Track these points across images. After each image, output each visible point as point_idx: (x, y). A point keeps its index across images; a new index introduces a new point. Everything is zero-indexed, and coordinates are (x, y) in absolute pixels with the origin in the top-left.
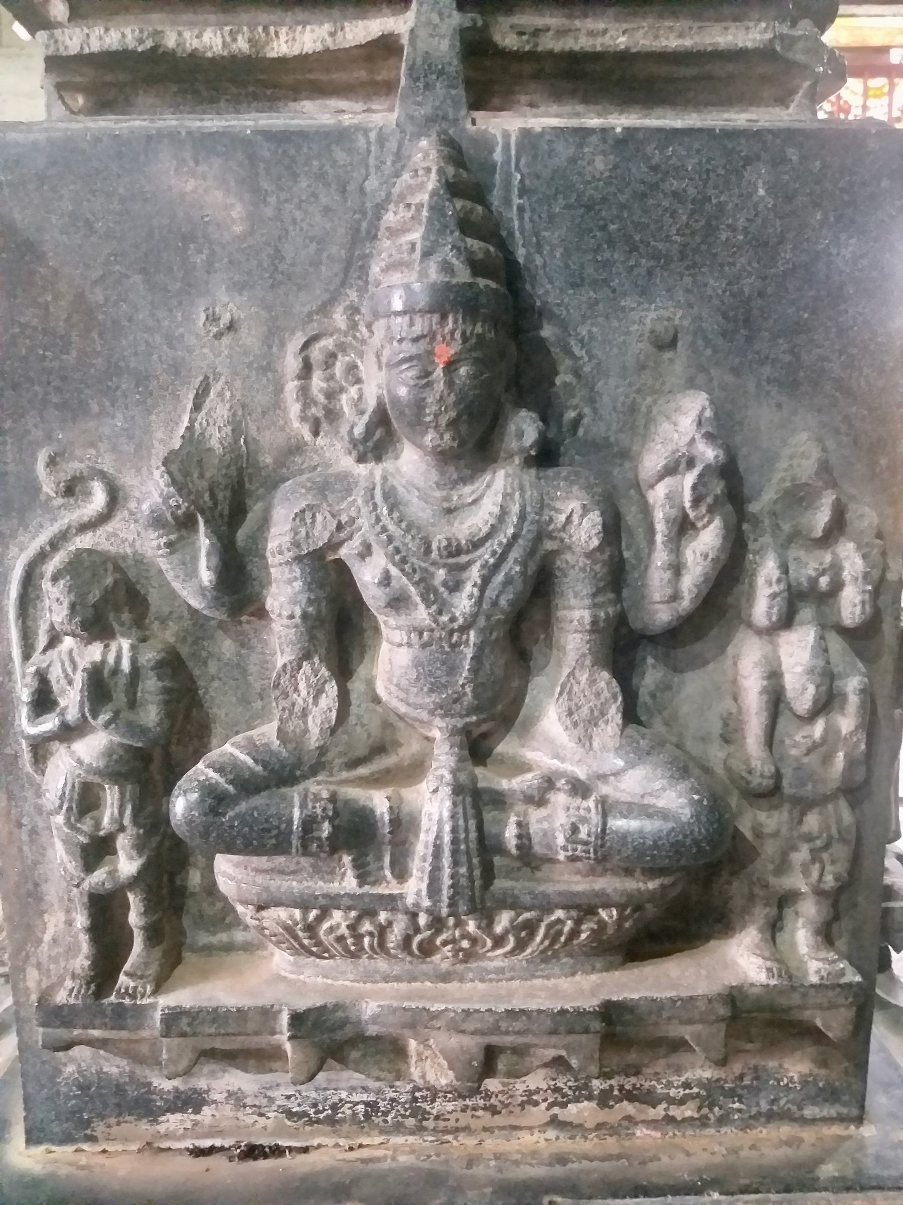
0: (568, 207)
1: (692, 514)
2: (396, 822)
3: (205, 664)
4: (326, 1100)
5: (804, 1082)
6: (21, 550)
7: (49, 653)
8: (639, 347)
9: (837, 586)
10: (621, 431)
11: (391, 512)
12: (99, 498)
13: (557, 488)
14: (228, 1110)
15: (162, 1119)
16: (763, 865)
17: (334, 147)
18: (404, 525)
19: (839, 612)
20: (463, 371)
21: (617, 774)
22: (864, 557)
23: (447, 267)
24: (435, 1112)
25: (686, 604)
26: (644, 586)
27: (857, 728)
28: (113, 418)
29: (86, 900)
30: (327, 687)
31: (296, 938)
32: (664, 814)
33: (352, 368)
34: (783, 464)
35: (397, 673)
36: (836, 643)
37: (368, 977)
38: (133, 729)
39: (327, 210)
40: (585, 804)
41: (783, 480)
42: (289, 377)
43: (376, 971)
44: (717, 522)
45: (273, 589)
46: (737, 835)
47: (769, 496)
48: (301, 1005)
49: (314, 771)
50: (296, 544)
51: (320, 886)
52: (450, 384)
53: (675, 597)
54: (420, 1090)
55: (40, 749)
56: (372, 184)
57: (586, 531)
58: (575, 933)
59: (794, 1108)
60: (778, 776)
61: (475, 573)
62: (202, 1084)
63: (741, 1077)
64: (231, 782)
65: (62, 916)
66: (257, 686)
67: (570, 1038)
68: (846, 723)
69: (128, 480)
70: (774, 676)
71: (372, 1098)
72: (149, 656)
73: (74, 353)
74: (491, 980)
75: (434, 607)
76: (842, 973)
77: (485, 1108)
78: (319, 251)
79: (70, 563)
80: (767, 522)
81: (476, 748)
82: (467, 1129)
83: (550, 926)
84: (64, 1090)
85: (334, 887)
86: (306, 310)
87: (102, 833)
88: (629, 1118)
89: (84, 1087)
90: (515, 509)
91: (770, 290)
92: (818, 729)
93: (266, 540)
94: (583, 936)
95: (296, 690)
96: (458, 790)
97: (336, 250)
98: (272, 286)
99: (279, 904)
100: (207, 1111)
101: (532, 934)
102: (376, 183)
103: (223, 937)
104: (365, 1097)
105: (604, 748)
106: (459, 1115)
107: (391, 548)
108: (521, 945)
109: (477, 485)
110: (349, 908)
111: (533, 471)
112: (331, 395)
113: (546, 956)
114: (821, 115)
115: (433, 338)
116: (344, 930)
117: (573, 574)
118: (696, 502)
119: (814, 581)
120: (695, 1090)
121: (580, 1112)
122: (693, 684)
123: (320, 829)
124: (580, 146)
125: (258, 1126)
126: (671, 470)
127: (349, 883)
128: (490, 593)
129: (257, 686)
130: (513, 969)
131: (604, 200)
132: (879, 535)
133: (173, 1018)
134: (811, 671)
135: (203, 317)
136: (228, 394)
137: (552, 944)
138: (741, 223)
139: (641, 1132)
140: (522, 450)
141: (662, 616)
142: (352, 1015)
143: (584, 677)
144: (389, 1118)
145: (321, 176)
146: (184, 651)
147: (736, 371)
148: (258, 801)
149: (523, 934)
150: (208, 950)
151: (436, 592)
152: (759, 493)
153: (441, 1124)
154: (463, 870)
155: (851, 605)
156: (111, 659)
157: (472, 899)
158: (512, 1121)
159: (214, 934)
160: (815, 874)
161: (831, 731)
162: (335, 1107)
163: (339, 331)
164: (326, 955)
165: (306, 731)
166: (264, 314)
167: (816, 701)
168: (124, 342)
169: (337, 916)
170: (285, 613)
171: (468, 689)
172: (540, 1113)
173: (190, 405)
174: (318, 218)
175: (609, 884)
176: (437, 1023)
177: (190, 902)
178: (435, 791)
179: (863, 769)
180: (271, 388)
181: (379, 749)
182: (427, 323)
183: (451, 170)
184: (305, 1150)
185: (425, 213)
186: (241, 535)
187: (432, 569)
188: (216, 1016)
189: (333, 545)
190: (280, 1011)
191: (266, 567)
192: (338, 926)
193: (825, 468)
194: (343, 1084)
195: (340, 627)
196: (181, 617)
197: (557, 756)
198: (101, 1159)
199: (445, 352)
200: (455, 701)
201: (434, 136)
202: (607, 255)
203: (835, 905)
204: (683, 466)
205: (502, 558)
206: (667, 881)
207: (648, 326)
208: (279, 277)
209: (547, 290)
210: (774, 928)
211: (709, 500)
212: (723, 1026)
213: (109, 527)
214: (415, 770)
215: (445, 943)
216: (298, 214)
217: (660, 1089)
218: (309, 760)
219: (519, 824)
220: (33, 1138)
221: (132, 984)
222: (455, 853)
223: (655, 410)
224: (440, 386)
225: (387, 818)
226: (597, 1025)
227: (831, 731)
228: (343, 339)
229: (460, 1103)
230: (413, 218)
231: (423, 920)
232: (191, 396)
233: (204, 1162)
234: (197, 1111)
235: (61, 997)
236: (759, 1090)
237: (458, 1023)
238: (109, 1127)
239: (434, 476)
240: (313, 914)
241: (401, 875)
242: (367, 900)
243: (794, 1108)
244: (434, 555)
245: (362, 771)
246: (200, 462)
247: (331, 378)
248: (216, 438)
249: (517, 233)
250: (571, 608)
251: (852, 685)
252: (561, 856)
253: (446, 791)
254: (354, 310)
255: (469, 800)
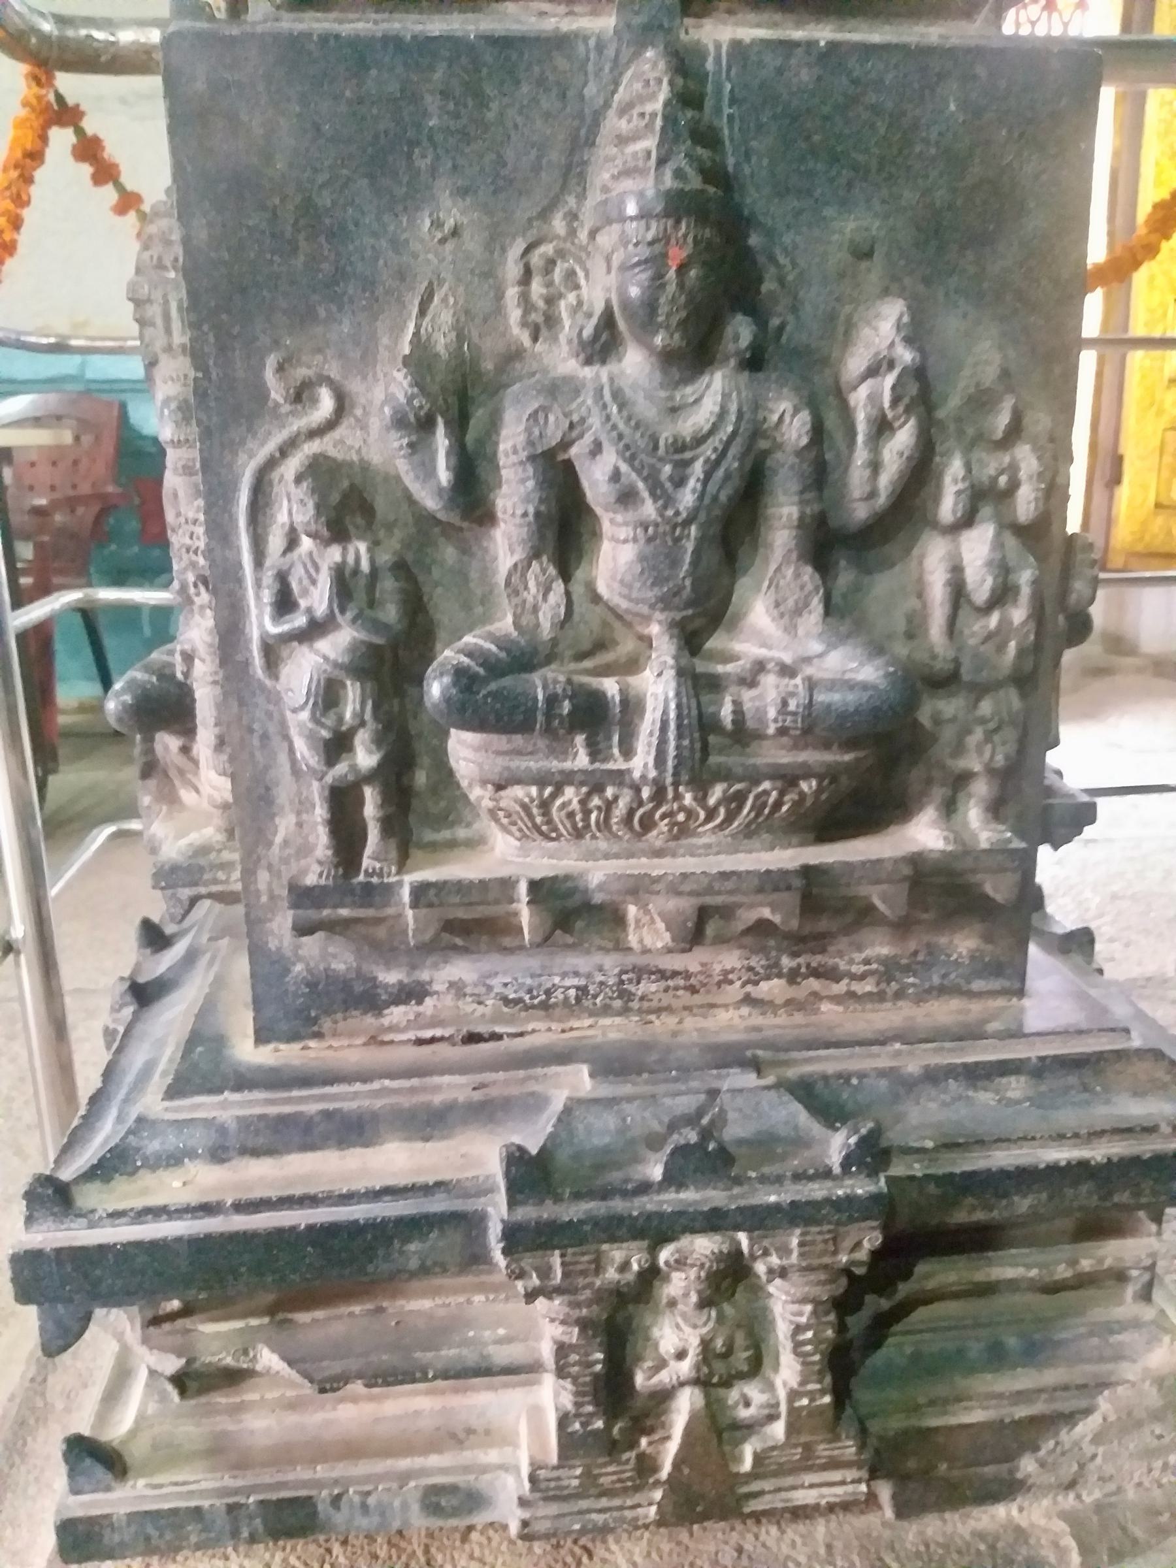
0: (775, 117)
1: (890, 415)
2: (625, 702)
3: (429, 571)
4: (540, 985)
5: (972, 958)
6: (251, 458)
7: (289, 556)
8: (838, 257)
9: (1014, 485)
10: (822, 338)
11: (620, 411)
12: (326, 403)
13: (769, 390)
14: (449, 1000)
15: (386, 1012)
16: (941, 750)
17: (554, 53)
18: (633, 423)
19: (1015, 511)
20: (693, 273)
21: (821, 656)
22: (1039, 458)
23: (679, 174)
24: (639, 993)
25: (882, 500)
26: (845, 485)
27: (1029, 617)
28: (340, 323)
29: (327, 793)
30: (554, 585)
31: (531, 816)
32: (865, 686)
33: (571, 275)
34: (966, 372)
35: (622, 569)
36: (1011, 541)
37: (591, 856)
38: (377, 626)
39: (547, 115)
40: (793, 682)
41: (967, 387)
42: (509, 283)
43: (597, 850)
44: (912, 422)
45: (505, 489)
46: (916, 724)
47: (954, 402)
48: (538, 876)
49: (549, 659)
50: (531, 443)
51: (555, 765)
52: (681, 285)
53: (872, 495)
54: (626, 972)
55: (272, 652)
56: (590, 90)
57: (795, 429)
58: (778, 804)
59: (962, 982)
60: (957, 662)
61: (698, 468)
62: (425, 976)
63: (915, 953)
64: (481, 665)
65: (292, 819)
66: (479, 592)
67: (775, 896)
68: (1018, 614)
69: (354, 386)
70: (957, 570)
71: (583, 982)
72: (385, 558)
73: (302, 258)
74: (700, 855)
75: (660, 502)
76: (1009, 841)
77: (685, 988)
78: (539, 158)
79: (310, 466)
80: (952, 427)
81: (691, 639)
82: (669, 1009)
83: (757, 797)
84: (292, 988)
85: (568, 765)
86: (528, 215)
87: (344, 728)
88: (815, 994)
89: (312, 985)
90: (733, 408)
91: (959, 202)
92: (994, 620)
93: (497, 444)
94: (785, 808)
95: (526, 588)
96: (681, 673)
97: (555, 156)
98: (495, 192)
99: (518, 781)
100: (429, 1002)
101: (740, 808)
102: (595, 90)
103: (446, 834)
104: (576, 981)
105: (808, 634)
106: (662, 995)
107: (621, 444)
108: (728, 820)
109: (696, 385)
110: (582, 784)
111: (746, 374)
112: (551, 301)
113: (749, 832)
114: (1008, 28)
115: (668, 243)
116: (575, 805)
117: (783, 472)
118: (895, 402)
119: (994, 480)
120: (874, 966)
121: (771, 989)
122: (882, 584)
123: (561, 707)
124: (788, 56)
125: (478, 1014)
126: (873, 371)
127: (582, 760)
128: (712, 488)
129: (479, 592)
130: (719, 844)
131: (808, 110)
132: (1052, 440)
133: (420, 892)
134: (989, 564)
135: (427, 223)
136: (451, 301)
137: (757, 816)
138: (933, 136)
139: (825, 1007)
140: (738, 353)
141: (861, 512)
142: (581, 884)
143: (789, 572)
144: (598, 1001)
145: (541, 82)
146: (410, 557)
147: (927, 281)
148: (507, 681)
149: (733, 805)
150: (433, 846)
151: (662, 486)
152: (945, 399)
153: (646, 1004)
154: (686, 742)
155: (1026, 503)
156: (351, 559)
157: (692, 769)
158: (710, 999)
159: (439, 831)
160: (987, 755)
161: (1004, 622)
162: (548, 993)
163: (557, 237)
164: (554, 835)
165: (538, 625)
166: (486, 220)
167: (993, 590)
168: (351, 247)
169: (569, 792)
170: (519, 512)
171: (688, 582)
172: (735, 991)
173: (415, 311)
174: (539, 123)
175: (811, 757)
176: (657, 887)
177: (415, 803)
178: (660, 675)
179: (1031, 659)
180: (492, 294)
181: (600, 646)
182: (662, 228)
183: (680, 81)
184: (521, 1034)
185: (659, 122)
186: (470, 438)
187: (659, 465)
188: (461, 887)
189: (565, 445)
190: (517, 881)
191: (497, 468)
192: (570, 802)
193: (1005, 374)
194: (556, 970)
195: (565, 529)
196: (406, 525)
197: (764, 645)
198: (330, 1053)
199: (677, 255)
200: (675, 594)
201: (662, 47)
202: (811, 164)
203: (1003, 786)
204: (885, 366)
205: (723, 455)
206: (861, 754)
207: (848, 236)
208: (501, 183)
209: (754, 199)
210: (949, 808)
211: (906, 400)
212: (906, 885)
213: (337, 434)
214: (632, 665)
215: (663, 817)
216: (520, 120)
217: (843, 966)
218: (544, 651)
219: (734, 702)
220: (262, 1036)
221: (378, 865)
222: (679, 726)
223: (855, 319)
224: (672, 288)
225: (617, 699)
226: (797, 883)
227: (1004, 622)
228: (562, 245)
229: (663, 984)
230: (646, 126)
231: (646, 793)
232: (417, 302)
233: (426, 1050)
234: (420, 1002)
235: (311, 880)
236: (933, 965)
237: (676, 886)
238: (336, 1022)
239: (658, 376)
240: (548, 791)
241: (628, 752)
242: (598, 775)
243: (962, 982)
244: (661, 451)
245: (588, 664)
246: (429, 366)
247: (549, 284)
248: (442, 343)
249: (727, 143)
250: (781, 505)
251: (1025, 578)
252: (771, 730)
253: (670, 674)
254: (573, 216)
255: (689, 683)
